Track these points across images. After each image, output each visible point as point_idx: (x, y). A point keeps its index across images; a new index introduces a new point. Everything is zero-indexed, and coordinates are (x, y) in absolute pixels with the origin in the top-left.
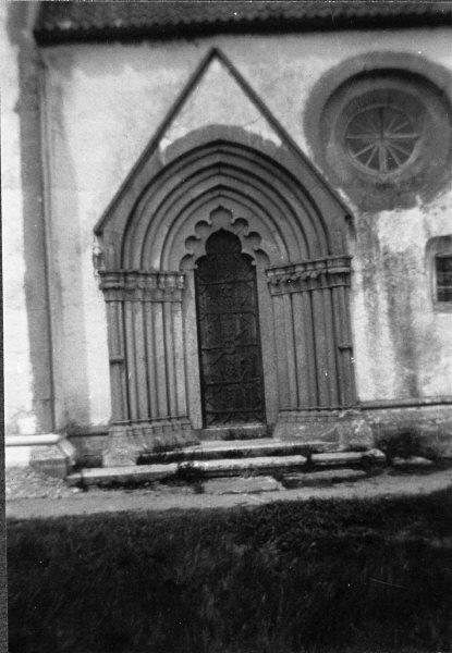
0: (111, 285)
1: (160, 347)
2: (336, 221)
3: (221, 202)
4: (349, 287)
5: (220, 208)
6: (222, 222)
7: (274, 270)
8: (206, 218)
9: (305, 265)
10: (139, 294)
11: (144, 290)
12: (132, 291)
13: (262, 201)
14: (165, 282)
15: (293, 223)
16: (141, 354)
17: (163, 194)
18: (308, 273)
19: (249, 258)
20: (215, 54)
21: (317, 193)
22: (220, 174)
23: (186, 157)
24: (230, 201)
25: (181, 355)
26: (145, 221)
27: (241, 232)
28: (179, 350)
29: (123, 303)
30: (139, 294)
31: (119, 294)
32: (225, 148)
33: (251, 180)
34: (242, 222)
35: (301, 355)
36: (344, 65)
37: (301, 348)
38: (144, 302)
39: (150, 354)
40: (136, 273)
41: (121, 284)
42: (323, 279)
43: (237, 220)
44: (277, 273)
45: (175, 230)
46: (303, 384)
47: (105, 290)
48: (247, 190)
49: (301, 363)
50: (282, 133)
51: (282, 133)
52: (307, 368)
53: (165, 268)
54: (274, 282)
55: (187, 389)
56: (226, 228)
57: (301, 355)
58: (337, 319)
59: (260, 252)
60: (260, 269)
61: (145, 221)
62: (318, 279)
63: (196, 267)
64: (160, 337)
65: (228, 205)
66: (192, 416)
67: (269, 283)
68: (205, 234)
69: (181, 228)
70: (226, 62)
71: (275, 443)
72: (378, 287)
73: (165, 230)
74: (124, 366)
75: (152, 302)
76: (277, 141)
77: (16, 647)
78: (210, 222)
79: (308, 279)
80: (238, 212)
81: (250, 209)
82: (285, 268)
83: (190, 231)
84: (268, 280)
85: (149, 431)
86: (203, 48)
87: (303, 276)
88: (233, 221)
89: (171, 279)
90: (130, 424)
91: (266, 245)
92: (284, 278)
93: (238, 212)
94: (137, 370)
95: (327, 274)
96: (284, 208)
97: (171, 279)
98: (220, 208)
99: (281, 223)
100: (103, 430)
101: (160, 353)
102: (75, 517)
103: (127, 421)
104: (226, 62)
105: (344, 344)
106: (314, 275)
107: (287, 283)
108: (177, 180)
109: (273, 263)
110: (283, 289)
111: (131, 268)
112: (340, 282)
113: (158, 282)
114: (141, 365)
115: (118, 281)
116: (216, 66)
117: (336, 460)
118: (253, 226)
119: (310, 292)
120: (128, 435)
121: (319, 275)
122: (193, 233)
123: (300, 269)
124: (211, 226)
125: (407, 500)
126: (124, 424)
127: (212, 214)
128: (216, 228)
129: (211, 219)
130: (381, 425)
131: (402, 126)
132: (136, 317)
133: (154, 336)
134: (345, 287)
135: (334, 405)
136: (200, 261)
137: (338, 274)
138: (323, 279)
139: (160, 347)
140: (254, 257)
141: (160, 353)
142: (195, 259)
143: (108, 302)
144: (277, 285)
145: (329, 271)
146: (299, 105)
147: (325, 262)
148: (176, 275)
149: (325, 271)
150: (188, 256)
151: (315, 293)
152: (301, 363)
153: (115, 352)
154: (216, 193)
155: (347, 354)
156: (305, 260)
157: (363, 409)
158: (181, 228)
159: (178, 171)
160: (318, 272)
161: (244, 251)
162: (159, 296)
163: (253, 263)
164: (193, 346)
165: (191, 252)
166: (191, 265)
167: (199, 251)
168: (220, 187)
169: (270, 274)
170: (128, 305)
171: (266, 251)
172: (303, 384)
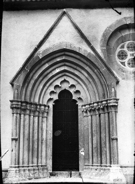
0: (14, 106)
1: (36, 135)
3: (65, 78)
4: (117, 112)
6: (65, 86)
7: (85, 106)
9: (98, 103)
10: (28, 112)
18: (99, 106)
19: (75, 101)
20: (64, 13)
22: (65, 65)
25: (45, 140)
26: (32, 82)
27: (72, 91)
28: (44, 137)
29: (20, 115)
30: (28, 112)
31: (19, 111)
34: (73, 86)
35: (95, 142)
38: (30, 116)
39: (31, 138)
42: (106, 109)
43: (76, 91)
47: (12, 108)
52: (97, 147)
53: (41, 103)
54: (85, 110)
55: (46, 154)
56: (67, 89)
59: (80, 99)
60: (80, 104)
61: (32, 82)
62: (103, 109)
63: (54, 104)
64: (36, 131)
65: (68, 79)
66: (48, 166)
67: (83, 111)
68: (58, 91)
70: (69, 17)
72: (123, 35)
78: (60, 86)
80: (72, 82)
81: (77, 81)
82: (90, 104)
83: (52, 89)
84: (83, 110)
85: (17, 171)
86: (60, 12)
89: (43, 107)
90: (18, 167)
92: (89, 109)
93: (72, 82)
95: (107, 107)
97: (43, 107)
101: (36, 138)
103: (17, 166)
104: (69, 17)
105: (114, 137)
107: (90, 111)
110: (89, 114)
112: (113, 110)
113: (36, 108)
116: (65, 18)
118: (78, 88)
120: (16, 172)
121: (104, 107)
124: (61, 87)
126: (15, 167)
132: (25, 119)
133: (33, 130)
134: (115, 112)
135: (108, 165)
136: (56, 102)
137: (112, 106)
138: (106, 109)
139: (36, 135)
140: (77, 101)
141: (36, 138)
142: (54, 100)
143: (13, 114)
144: (86, 112)
145: (109, 105)
146: (100, 37)
147: (107, 101)
148: (45, 106)
151: (102, 115)
153: (14, 135)
155: (115, 141)
156: (98, 100)
159: (47, 62)
160: (104, 105)
163: (77, 103)
164: (50, 136)
168: (65, 71)
169: (83, 107)
170: (22, 115)
171: (82, 98)
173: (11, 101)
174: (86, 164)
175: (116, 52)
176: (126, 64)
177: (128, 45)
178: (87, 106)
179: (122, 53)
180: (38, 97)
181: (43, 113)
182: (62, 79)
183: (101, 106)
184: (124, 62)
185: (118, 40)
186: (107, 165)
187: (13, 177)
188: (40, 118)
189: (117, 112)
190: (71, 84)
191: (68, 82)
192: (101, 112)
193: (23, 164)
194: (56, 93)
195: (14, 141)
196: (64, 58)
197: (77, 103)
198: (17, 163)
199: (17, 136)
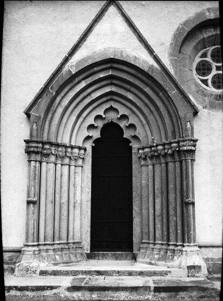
2: (188, 115)
3: (112, 104)
6: (112, 116)
7: (143, 148)
8: (102, 113)
9: (164, 145)
10: (53, 158)
11: (56, 156)
12: (47, 155)
13: (139, 103)
14: (72, 153)
15: (158, 118)
16: (50, 198)
17: (72, 94)
19: (128, 141)
21: (173, 93)
22: (112, 84)
23: (87, 70)
26: (60, 110)
27: (123, 124)
29: (41, 163)
30: (53, 158)
32: (115, 65)
33: (133, 89)
34: (124, 117)
35: (158, 207)
36: (198, 15)
37: (158, 201)
39: (57, 199)
40: (51, 144)
44: (146, 150)
45: (81, 119)
46: (158, 226)
48: (130, 96)
49: (158, 212)
50: (156, 59)
51: (156, 59)
54: (143, 156)
56: (115, 121)
57: (158, 207)
58: (184, 183)
60: (135, 145)
61: (60, 110)
62: (172, 155)
65: (116, 106)
67: (139, 158)
68: (100, 124)
69: (85, 118)
71: (139, 266)
73: (74, 118)
74: (37, 206)
75: (47, 163)
76: (152, 62)
78: (104, 116)
79: (165, 155)
80: (123, 111)
81: (130, 109)
83: (91, 121)
84: (139, 156)
87: (163, 153)
88: (119, 116)
89: (76, 151)
91: (140, 132)
92: (149, 154)
93: (123, 111)
94: (46, 208)
96: (152, 108)
99: (151, 118)
100: (18, 249)
103: (35, 244)
106: (170, 151)
107: (152, 158)
108: (83, 84)
109: (144, 144)
110: (149, 162)
111: (48, 138)
114: (50, 206)
117: (189, 172)
118: (132, 120)
119: (167, 164)
121: (173, 152)
122: (92, 122)
123: (160, 147)
124: (105, 118)
127: (106, 111)
130: (212, 259)
136: (96, 141)
139: (65, 195)
144: (145, 159)
147: (178, 142)
148: (80, 148)
149: (177, 149)
150: (88, 138)
152: (158, 212)
156: (164, 141)
157: (200, 247)
158: (85, 118)
159: (84, 79)
160: (173, 149)
162: (67, 161)
166: (89, 146)
167: (96, 134)
170: (44, 164)
172: (158, 226)
179: (204, 65)
182: (107, 106)
191: (116, 111)
194: (97, 127)
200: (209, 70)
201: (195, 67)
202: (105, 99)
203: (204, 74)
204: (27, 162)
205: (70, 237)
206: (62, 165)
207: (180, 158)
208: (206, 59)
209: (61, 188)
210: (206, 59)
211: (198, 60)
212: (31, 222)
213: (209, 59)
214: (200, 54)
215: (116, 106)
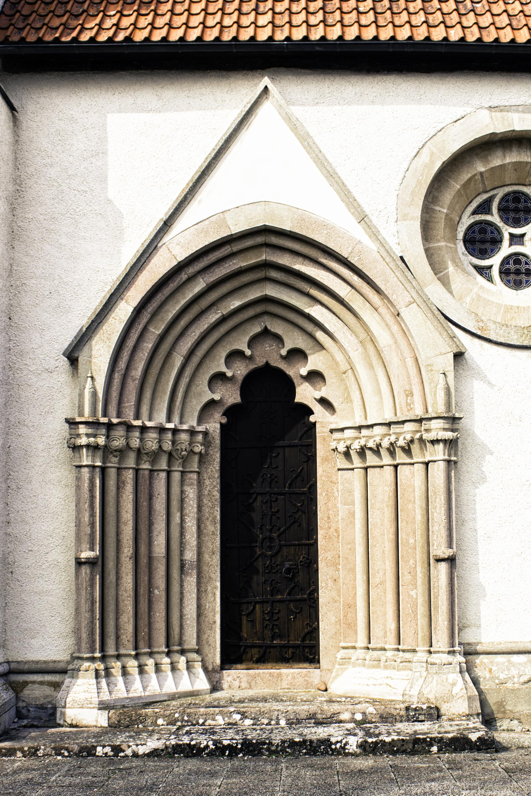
5: (266, 333)
24: (280, 322)
32: (274, 240)
41: (101, 441)
56: (273, 363)
59: (324, 402)
65: (277, 327)
77: (530, 112)
78: (248, 352)
88: (284, 352)
98: (266, 333)
102: (103, 180)
115: (95, 436)
122: (208, 396)
125: (285, 662)
128: (260, 362)
129: (249, 347)
131: (57, 730)
139: (160, 542)
150: (211, 404)
154: (259, 309)
161: (298, 399)
165: (217, 397)
173: (72, 423)
174: (342, 644)
175: (459, 229)
176: (495, 272)
177: (502, 199)
178: (348, 433)
179: (483, 231)
180: (166, 405)
181: (185, 460)
182: (257, 329)
183: (401, 438)
184: (490, 267)
185: (466, 185)
186: (387, 647)
187: (24, 701)
188: (176, 476)
189: (455, 463)
190: (289, 345)
191: (279, 339)
192: (401, 457)
193: (117, 649)
194: (232, 379)
195: (85, 570)
196: (264, 257)
197: (312, 419)
198: (84, 645)
199: (97, 547)
200: (497, 242)
201: (460, 235)
202: (251, 312)
203: (483, 254)
204: (367, 214)
205: (172, 641)
206: (366, 469)
207: (138, 463)
208: (488, 218)
209: (182, 534)
210: (488, 218)
211: (467, 221)
212: (84, 623)
213: (495, 218)
214: (474, 205)
215: (277, 327)
